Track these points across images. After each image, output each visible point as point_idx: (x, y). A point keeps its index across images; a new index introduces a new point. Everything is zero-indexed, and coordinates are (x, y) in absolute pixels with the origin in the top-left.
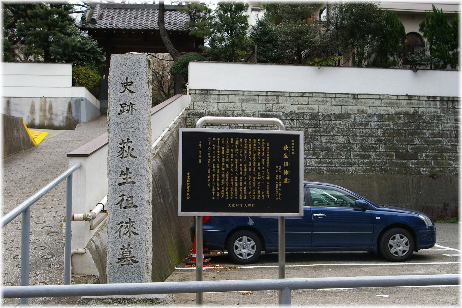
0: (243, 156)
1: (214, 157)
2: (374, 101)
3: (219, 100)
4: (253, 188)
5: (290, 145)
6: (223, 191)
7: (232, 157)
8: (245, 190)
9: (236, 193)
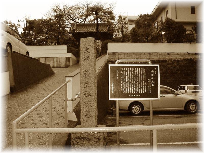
0: (135, 75)
1: (123, 76)
2: (175, 55)
3: (119, 56)
4: (139, 88)
5: (154, 71)
6: (127, 90)
7: (130, 76)
8: (136, 89)
9: (132, 90)
